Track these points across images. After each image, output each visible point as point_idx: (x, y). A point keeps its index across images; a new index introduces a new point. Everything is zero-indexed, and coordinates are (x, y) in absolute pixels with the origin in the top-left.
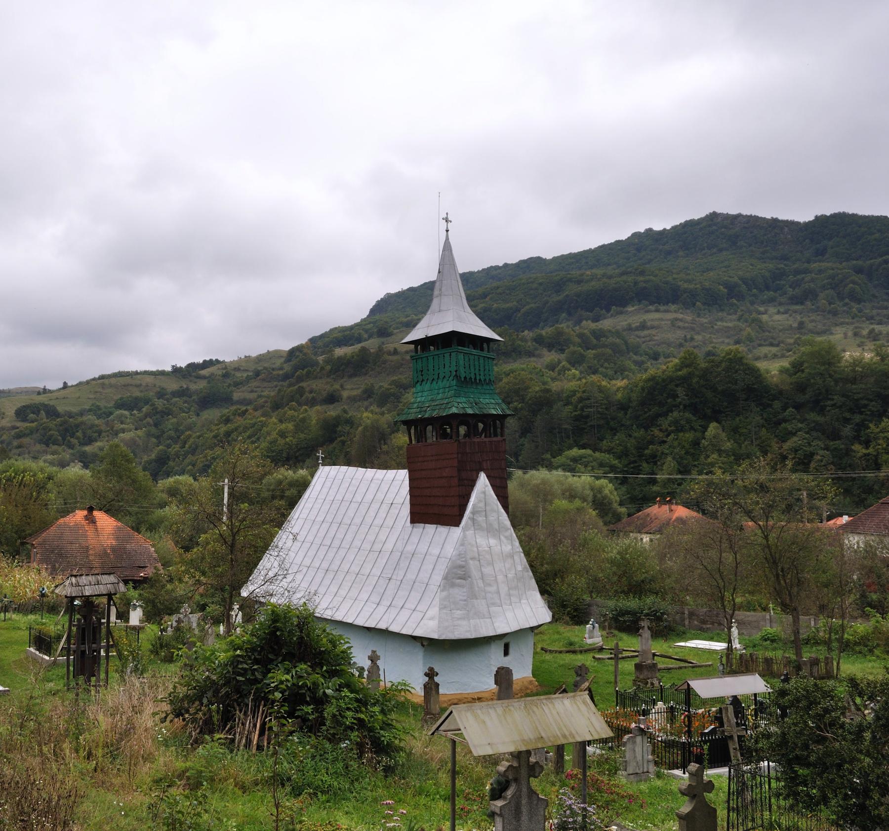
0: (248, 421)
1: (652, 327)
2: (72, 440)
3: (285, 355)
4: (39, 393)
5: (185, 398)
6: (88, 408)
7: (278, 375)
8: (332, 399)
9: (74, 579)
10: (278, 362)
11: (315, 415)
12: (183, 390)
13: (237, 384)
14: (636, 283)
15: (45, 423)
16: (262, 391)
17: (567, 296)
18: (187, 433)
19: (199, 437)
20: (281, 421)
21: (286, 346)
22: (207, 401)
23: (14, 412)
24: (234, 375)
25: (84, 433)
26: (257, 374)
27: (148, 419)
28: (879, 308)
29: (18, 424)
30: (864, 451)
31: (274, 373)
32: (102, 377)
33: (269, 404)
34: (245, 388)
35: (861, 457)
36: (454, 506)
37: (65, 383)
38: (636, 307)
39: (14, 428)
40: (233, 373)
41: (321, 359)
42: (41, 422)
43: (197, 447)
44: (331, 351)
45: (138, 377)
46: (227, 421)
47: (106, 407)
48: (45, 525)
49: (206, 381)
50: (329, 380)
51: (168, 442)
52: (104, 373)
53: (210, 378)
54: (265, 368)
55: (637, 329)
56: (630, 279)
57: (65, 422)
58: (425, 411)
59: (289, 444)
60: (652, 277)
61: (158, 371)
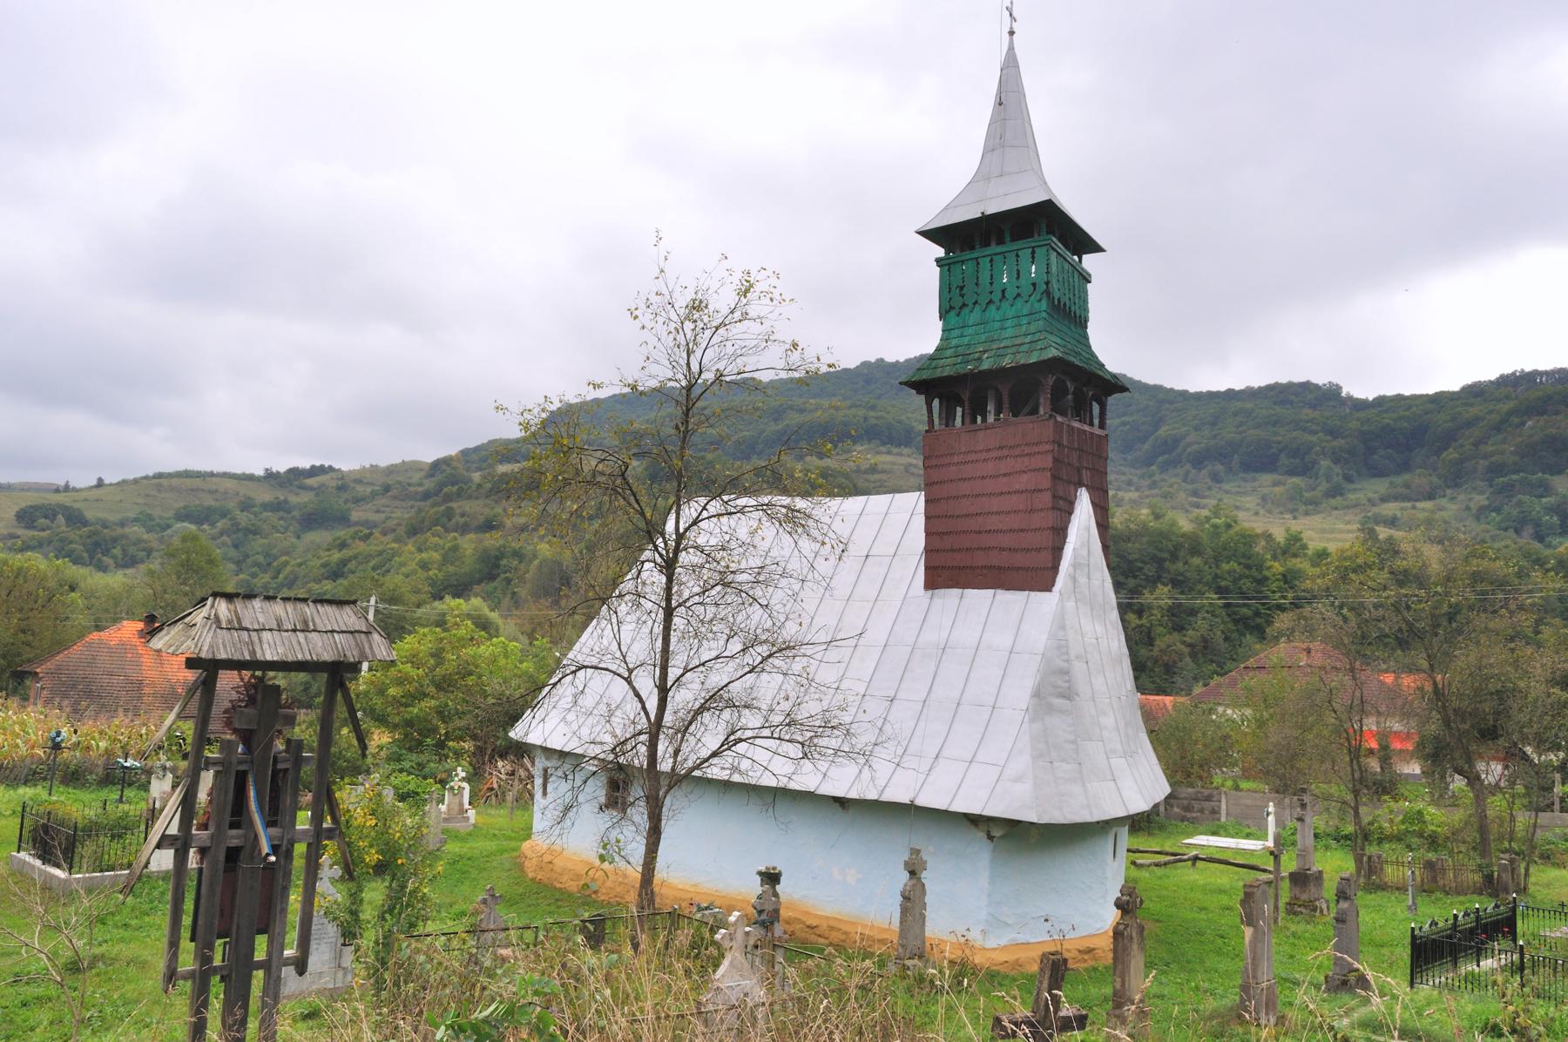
0: (374, 548)
1: (884, 472)
2: (105, 558)
3: (427, 467)
4: (57, 491)
5: (281, 513)
6: (133, 516)
7: (417, 493)
8: (489, 526)
9: (223, 607)
10: (417, 477)
11: (469, 544)
12: (279, 503)
13: (357, 501)
14: (866, 419)
15: (63, 532)
16: (392, 512)
17: (787, 425)
18: (284, 558)
19: (300, 565)
20: (420, 550)
21: (429, 454)
22: (312, 520)
23: (14, 513)
24: (354, 488)
25: (124, 550)
26: (387, 489)
27: (225, 538)
28: (1118, 474)
29: (20, 532)
30: (1137, 622)
31: (411, 489)
32: (159, 476)
33: (403, 528)
34: (369, 506)
35: (1133, 629)
36: (1039, 550)
37: (100, 480)
38: (866, 446)
39: (13, 536)
40: (352, 485)
41: (476, 477)
42: (58, 530)
43: (296, 578)
44: (491, 466)
45: (214, 479)
46: (343, 545)
47: (161, 518)
48: (60, 645)
49: (313, 493)
50: (487, 501)
51: (254, 570)
52: (162, 471)
53: (319, 490)
54: (399, 483)
55: (866, 472)
56: (861, 412)
57: (95, 533)
58: (979, 359)
59: (432, 580)
60: (883, 413)
61: (244, 474)
